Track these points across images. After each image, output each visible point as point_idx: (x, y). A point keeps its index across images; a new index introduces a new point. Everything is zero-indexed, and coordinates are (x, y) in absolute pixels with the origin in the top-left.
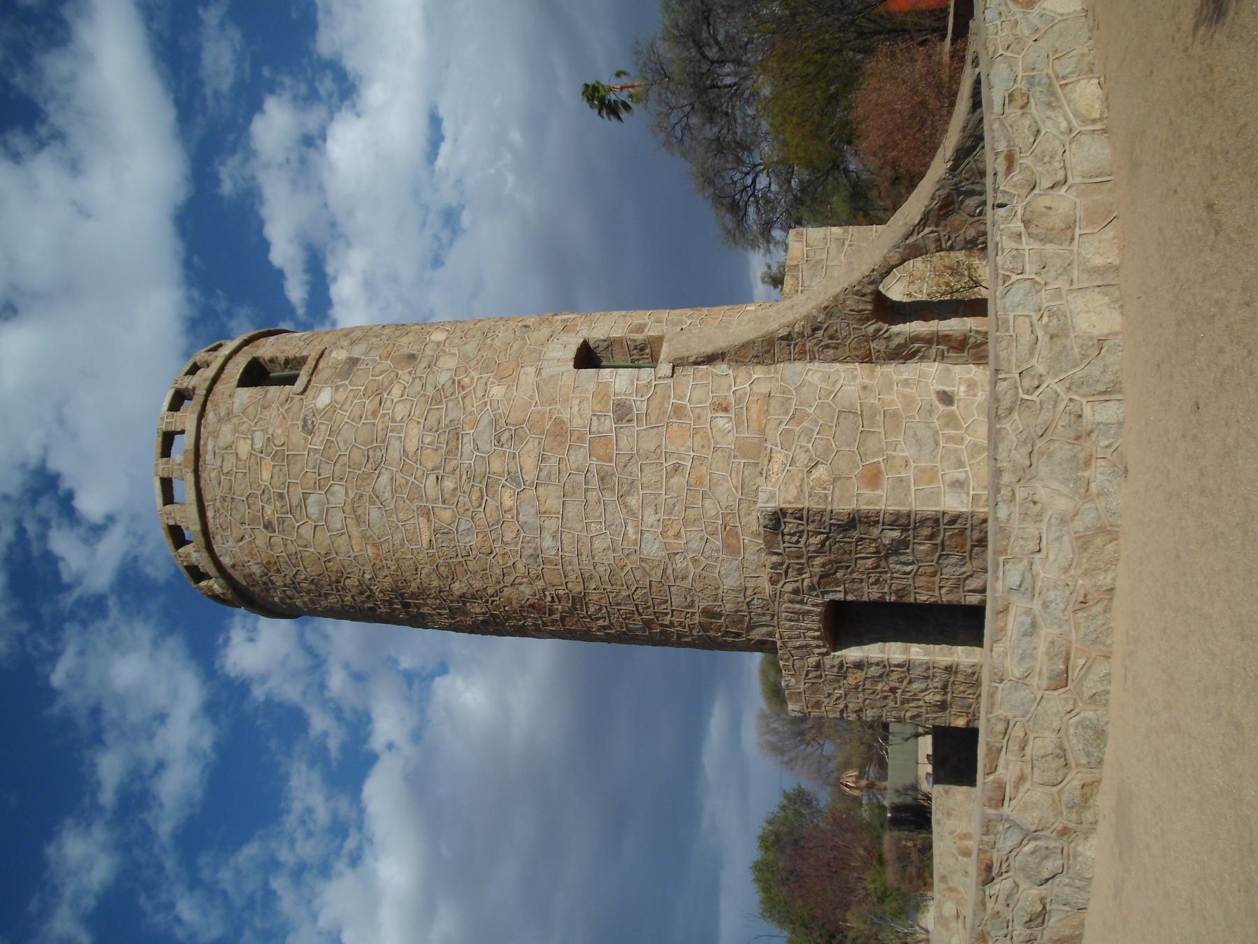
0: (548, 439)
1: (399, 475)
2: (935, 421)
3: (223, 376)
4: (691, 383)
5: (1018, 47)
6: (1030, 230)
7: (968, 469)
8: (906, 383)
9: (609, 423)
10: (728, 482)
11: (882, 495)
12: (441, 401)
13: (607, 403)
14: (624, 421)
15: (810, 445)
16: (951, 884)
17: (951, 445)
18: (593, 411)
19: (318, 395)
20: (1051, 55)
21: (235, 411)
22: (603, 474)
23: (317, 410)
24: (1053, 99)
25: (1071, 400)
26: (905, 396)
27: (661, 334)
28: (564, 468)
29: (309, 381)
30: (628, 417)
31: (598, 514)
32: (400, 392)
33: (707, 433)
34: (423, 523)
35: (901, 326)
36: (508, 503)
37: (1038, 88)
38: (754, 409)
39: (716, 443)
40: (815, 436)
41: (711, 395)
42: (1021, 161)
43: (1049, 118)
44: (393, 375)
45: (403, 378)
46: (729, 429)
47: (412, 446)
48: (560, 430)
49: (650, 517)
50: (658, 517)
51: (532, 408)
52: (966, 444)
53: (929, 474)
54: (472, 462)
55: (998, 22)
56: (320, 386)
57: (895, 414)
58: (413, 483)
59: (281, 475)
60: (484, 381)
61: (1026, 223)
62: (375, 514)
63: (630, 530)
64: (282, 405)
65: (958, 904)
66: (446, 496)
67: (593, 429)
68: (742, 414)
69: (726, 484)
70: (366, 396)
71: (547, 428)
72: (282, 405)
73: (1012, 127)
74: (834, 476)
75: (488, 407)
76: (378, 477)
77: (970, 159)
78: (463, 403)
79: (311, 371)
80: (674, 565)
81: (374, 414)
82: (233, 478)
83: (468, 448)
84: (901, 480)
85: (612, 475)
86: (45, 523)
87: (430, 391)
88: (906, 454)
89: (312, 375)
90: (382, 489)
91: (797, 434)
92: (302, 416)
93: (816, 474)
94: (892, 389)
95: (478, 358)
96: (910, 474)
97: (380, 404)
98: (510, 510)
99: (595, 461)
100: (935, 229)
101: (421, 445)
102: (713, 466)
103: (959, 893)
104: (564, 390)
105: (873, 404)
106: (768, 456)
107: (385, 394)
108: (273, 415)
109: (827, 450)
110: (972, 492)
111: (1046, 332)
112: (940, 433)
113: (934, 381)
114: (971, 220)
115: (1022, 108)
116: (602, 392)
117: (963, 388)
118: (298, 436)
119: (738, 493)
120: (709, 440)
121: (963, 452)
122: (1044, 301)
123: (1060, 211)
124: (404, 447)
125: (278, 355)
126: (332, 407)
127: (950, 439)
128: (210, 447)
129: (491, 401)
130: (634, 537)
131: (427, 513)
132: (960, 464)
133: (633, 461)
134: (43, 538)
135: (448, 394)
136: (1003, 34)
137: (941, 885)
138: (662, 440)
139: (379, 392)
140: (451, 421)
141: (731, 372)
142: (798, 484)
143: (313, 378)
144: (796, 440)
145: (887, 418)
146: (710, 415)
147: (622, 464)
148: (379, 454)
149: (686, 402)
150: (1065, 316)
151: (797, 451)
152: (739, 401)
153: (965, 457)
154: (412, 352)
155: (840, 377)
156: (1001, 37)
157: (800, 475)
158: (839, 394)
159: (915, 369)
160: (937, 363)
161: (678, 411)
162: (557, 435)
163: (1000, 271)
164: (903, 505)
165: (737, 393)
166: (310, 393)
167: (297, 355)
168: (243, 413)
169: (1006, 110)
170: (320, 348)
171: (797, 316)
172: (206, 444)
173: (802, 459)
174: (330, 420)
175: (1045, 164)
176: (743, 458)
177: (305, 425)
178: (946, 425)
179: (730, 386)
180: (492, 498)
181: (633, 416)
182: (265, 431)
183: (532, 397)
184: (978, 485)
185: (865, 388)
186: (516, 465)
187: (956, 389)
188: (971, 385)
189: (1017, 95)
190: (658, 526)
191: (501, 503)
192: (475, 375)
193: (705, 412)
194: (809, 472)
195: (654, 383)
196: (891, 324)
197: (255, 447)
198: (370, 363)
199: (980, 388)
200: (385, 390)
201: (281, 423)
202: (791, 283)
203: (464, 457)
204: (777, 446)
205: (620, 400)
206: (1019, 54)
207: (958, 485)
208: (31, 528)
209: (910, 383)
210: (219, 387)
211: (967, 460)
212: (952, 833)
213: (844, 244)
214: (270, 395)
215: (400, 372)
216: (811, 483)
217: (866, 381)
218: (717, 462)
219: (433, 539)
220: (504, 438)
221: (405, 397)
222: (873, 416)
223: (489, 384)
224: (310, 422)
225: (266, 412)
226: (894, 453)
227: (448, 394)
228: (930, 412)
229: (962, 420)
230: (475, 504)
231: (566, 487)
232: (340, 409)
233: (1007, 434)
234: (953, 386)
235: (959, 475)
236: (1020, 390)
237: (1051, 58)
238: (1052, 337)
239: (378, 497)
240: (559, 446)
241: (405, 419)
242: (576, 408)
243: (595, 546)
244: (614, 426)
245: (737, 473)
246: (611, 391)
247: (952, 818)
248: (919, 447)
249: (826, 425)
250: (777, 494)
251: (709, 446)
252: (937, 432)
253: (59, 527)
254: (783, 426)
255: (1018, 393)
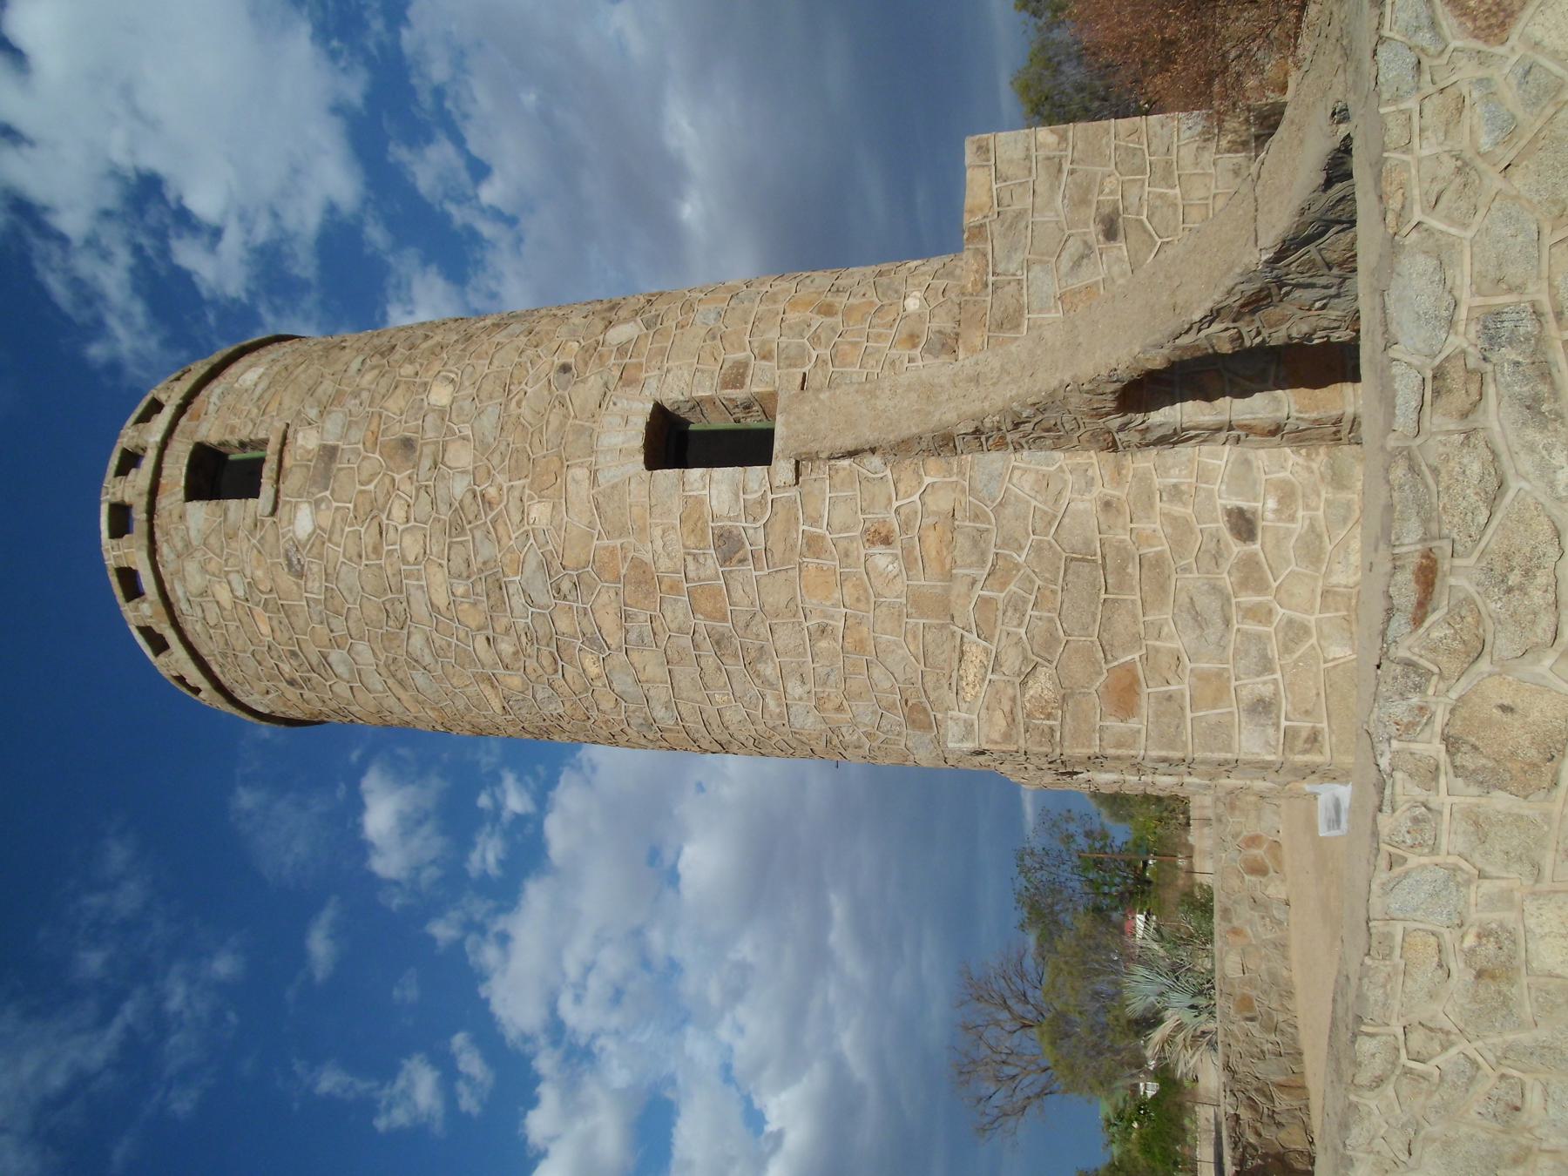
0: (627, 588)
1: (435, 635)
2: (1225, 575)
3: (163, 481)
4: (828, 495)
5: (1464, 205)
6: (1458, 760)
7: (1278, 676)
8: (1176, 492)
9: (711, 564)
10: (902, 648)
11: (1139, 731)
12: (463, 528)
13: (703, 537)
14: (735, 560)
15: (1022, 631)
16: (1236, 923)
17: (1251, 627)
18: (685, 547)
19: (295, 517)
20: (1547, 230)
21: (195, 543)
22: (717, 637)
23: (299, 541)
24: (1544, 389)
25: (1503, 1076)
26: (1173, 520)
27: (770, 389)
28: (660, 628)
29: (277, 491)
30: (739, 556)
31: (722, 684)
32: (403, 514)
33: (860, 579)
34: (488, 691)
35: (1166, 410)
36: (593, 670)
37: (1510, 354)
38: (932, 539)
39: (877, 595)
40: (1029, 612)
41: (861, 517)
42: (1452, 581)
43: (1531, 448)
44: (387, 481)
45: (402, 488)
46: (895, 573)
47: (441, 599)
48: (644, 577)
49: (795, 689)
50: (807, 688)
51: (595, 542)
52: (1275, 624)
53: (1215, 686)
54: (529, 621)
55: (1411, 104)
56: (293, 500)
57: (1159, 561)
58: (457, 646)
59: (282, 628)
60: (516, 494)
61: (1451, 743)
62: (420, 679)
63: (771, 703)
64: (251, 533)
65: (1244, 953)
66: (507, 661)
67: (691, 575)
68: (914, 547)
69: (900, 651)
70: (359, 520)
71: (623, 572)
72: (251, 533)
73: (1435, 471)
74: (1063, 691)
75: (532, 540)
76: (408, 638)
77: (1311, 247)
78: (496, 534)
79: (275, 476)
80: (841, 737)
81: (376, 550)
82: (224, 632)
83: (518, 601)
84: (1170, 698)
85: (731, 637)
86: (161, 235)
87: (445, 514)
88: (1176, 644)
89: (277, 481)
90: (419, 653)
91: (1001, 607)
92: (282, 551)
93: (1034, 689)
94: (1152, 506)
95: (502, 448)
96: (1182, 687)
97: (381, 533)
98: (599, 677)
99: (701, 622)
100: (1231, 325)
101: (452, 598)
102: (877, 628)
103: (1245, 936)
104: (635, 510)
105: (1122, 541)
106: (957, 650)
107: (384, 517)
108: (244, 549)
109: (1051, 641)
110: (1284, 723)
111: (1468, 964)
112: (1234, 601)
113: (1224, 487)
114: (1301, 314)
115: (1464, 415)
116: (693, 514)
117: (1271, 504)
118: (286, 580)
119: (919, 663)
120: (866, 590)
121: (1269, 638)
122: (1473, 909)
123: (1535, 715)
124: (430, 599)
125: (228, 437)
126: (321, 536)
127: (1250, 613)
128: (180, 592)
129: (533, 530)
130: (778, 710)
131: (491, 681)
132: (1266, 666)
133: (758, 618)
134: (165, 252)
135: (471, 517)
136: (1425, 152)
137: (1223, 924)
138: (794, 589)
139: (374, 511)
140: (484, 563)
141: (888, 472)
142: (1007, 709)
143: (282, 486)
144: (1000, 622)
145: (1146, 567)
146: (863, 552)
147: (741, 624)
148: (400, 608)
149: (822, 531)
150: (1514, 942)
151: (1003, 643)
152: (906, 526)
153: (1273, 649)
154: (408, 434)
155: (1065, 482)
156: (1420, 161)
157: (1010, 691)
158: (1066, 520)
159: (1190, 461)
160: (1227, 447)
161: (814, 544)
162: (640, 582)
163: (1384, 847)
164: (1174, 749)
165: (902, 511)
166: (283, 511)
167: (253, 437)
168: (205, 544)
169: (1426, 424)
170: (280, 426)
171: (986, 405)
172: (173, 589)
173: (1012, 661)
174: (321, 556)
175: (1509, 590)
176: (922, 616)
177: (290, 565)
178: (1244, 584)
179: (890, 500)
180: (571, 663)
181: (746, 554)
182: (241, 572)
183: (591, 525)
184: (1295, 709)
185: (1107, 505)
186: (591, 623)
187: (1260, 505)
188: (1287, 495)
189: (1456, 376)
190: (809, 699)
191: (584, 671)
192: (500, 479)
193: (855, 545)
194: (1023, 683)
195: (770, 497)
196: (1147, 410)
197: (237, 594)
198: (353, 458)
199: (1300, 502)
200: (382, 511)
201: (259, 561)
202: (975, 267)
203: (516, 613)
204: (970, 631)
205: (722, 527)
206: (1465, 226)
207: (1262, 708)
208: (145, 241)
209: (1183, 493)
210: (163, 502)
211: (1277, 656)
212: (1235, 836)
213: (1060, 170)
214: (232, 515)
215: (397, 477)
216: (1028, 705)
217: (1110, 491)
218: (883, 622)
219: (506, 705)
220: (566, 586)
221: (412, 523)
222: (1121, 569)
223: (525, 499)
224: (295, 561)
225: (233, 545)
226: (1158, 643)
227: (471, 517)
228: (1217, 558)
229: (1269, 572)
230: (550, 670)
231: (669, 652)
232: (330, 540)
233: (1370, 1113)
234: (1255, 500)
235: (1261, 687)
236: (1403, 1052)
237: (1548, 240)
238: (1480, 974)
239: (416, 661)
240: (645, 598)
241: (420, 558)
242: (659, 543)
243: (727, 718)
244: (720, 570)
245: (915, 637)
246: (707, 509)
247: (1237, 813)
248: (1198, 632)
249: (1046, 588)
250: (976, 727)
251: (868, 600)
252: (1229, 600)
253: (179, 236)
254: (978, 591)
255: (1398, 1057)
